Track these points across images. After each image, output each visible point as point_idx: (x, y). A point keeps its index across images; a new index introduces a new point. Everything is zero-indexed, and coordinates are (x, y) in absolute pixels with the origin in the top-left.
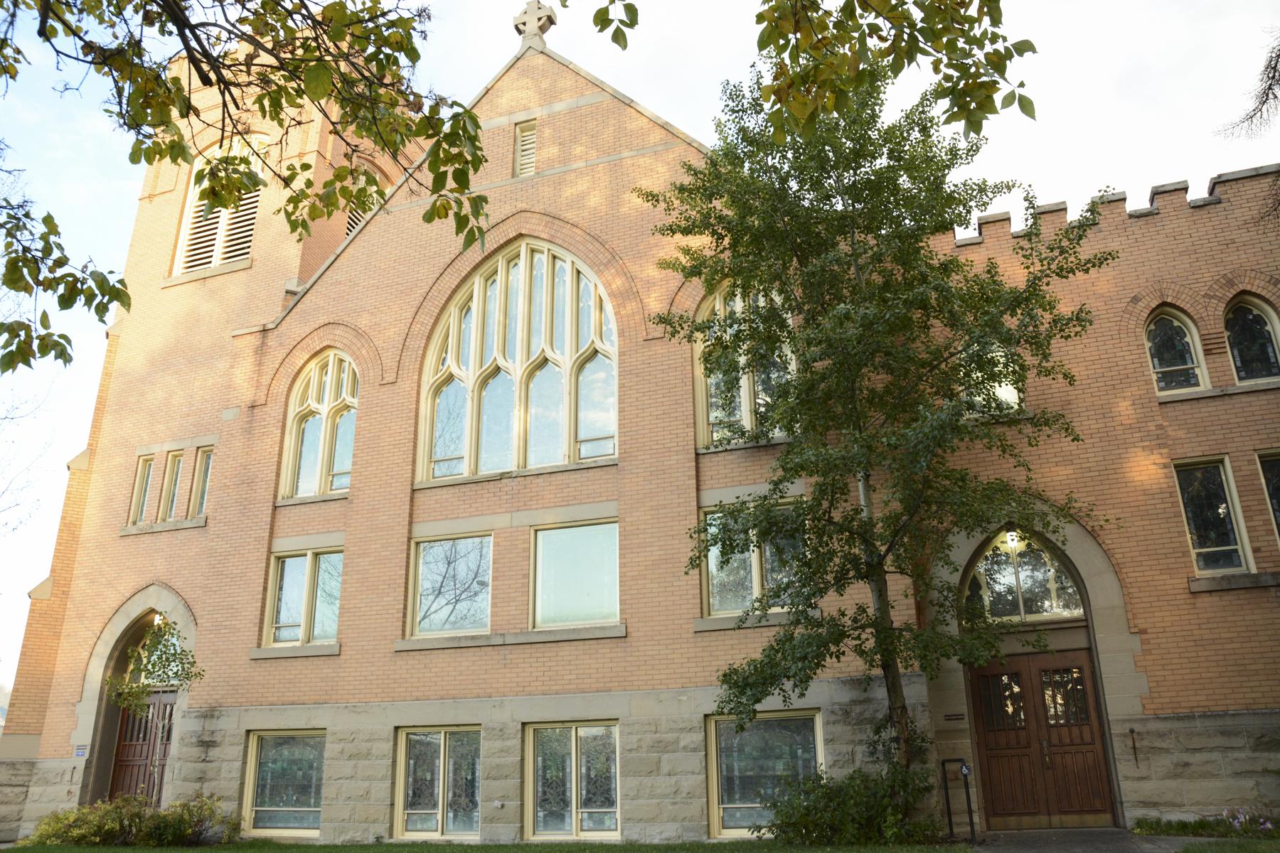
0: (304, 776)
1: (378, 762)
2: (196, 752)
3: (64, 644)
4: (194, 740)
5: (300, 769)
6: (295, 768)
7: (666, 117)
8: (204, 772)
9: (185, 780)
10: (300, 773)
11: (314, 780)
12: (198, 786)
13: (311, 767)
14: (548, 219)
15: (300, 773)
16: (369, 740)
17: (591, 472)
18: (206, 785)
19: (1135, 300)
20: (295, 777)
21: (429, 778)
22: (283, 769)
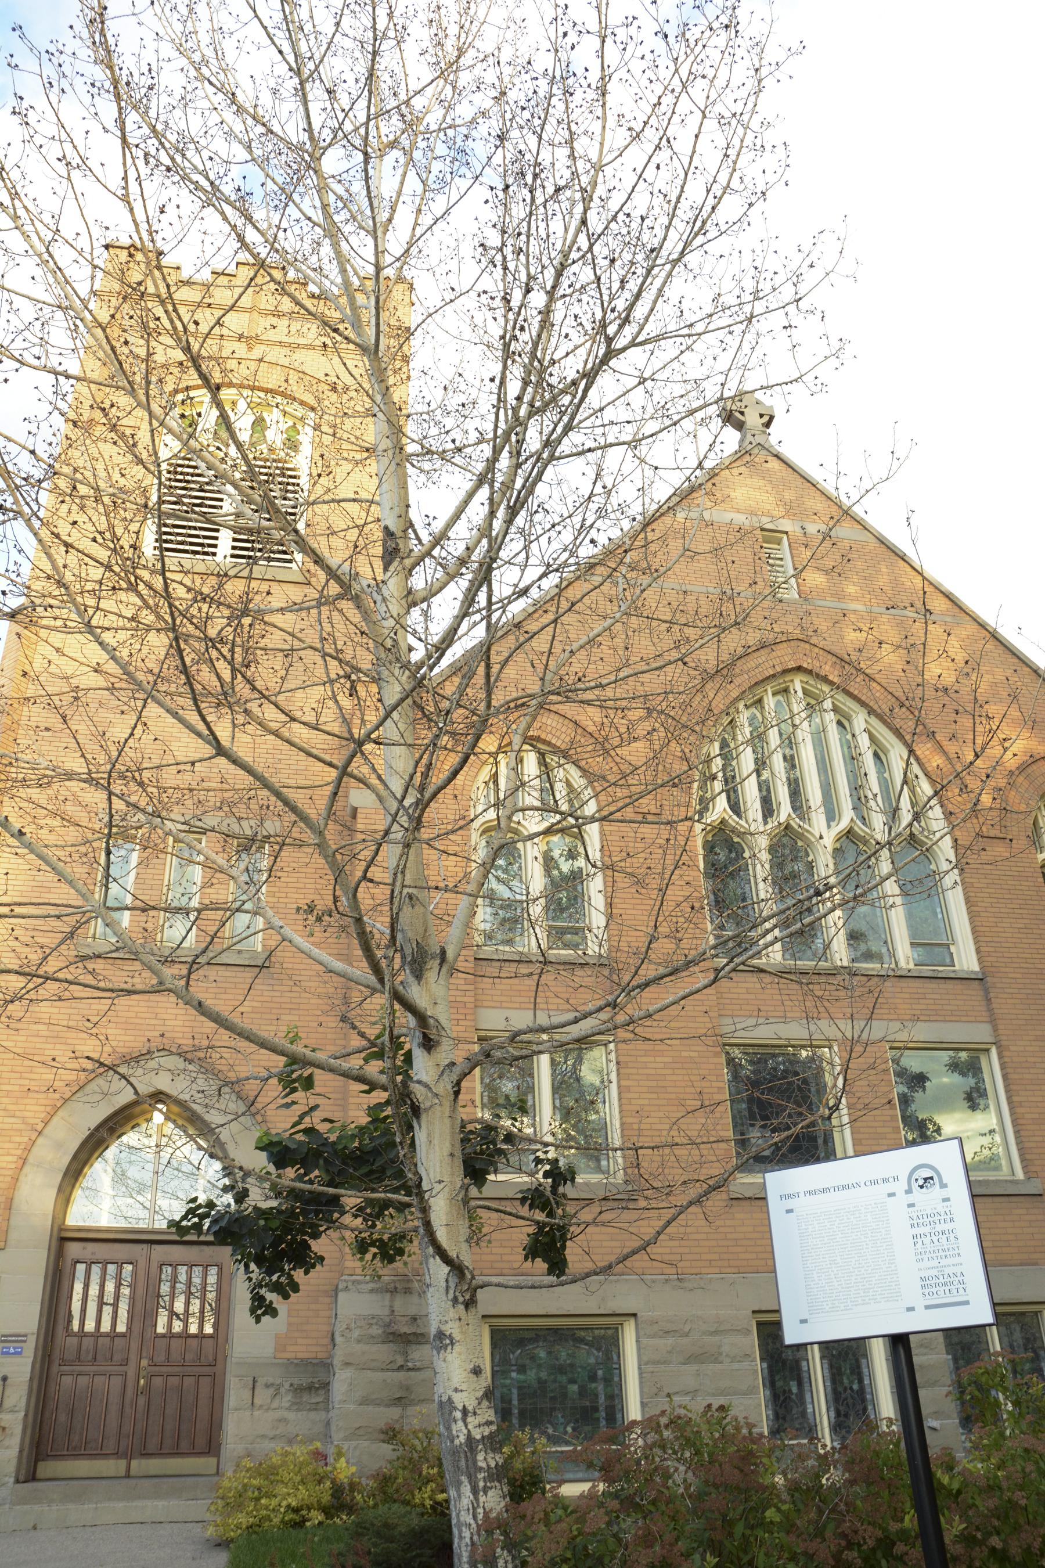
0: (583, 1392)
1: (736, 1366)
2: (383, 1352)
3: (131, 1134)
4: (376, 1331)
5: (573, 1381)
6: (564, 1379)
7: (949, 586)
8: (408, 1388)
9: (365, 1401)
10: (574, 1388)
11: (602, 1399)
12: (395, 1412)
13: (593, 1378)
14: (834, 659)
15: (574, 1388)
16: (716, 1333)
17: (950, 985)
18: (412, 1410)
19: (452, 1155)
20: (565, 1395)
21: (855, 1387)
22: (540, 1381)
